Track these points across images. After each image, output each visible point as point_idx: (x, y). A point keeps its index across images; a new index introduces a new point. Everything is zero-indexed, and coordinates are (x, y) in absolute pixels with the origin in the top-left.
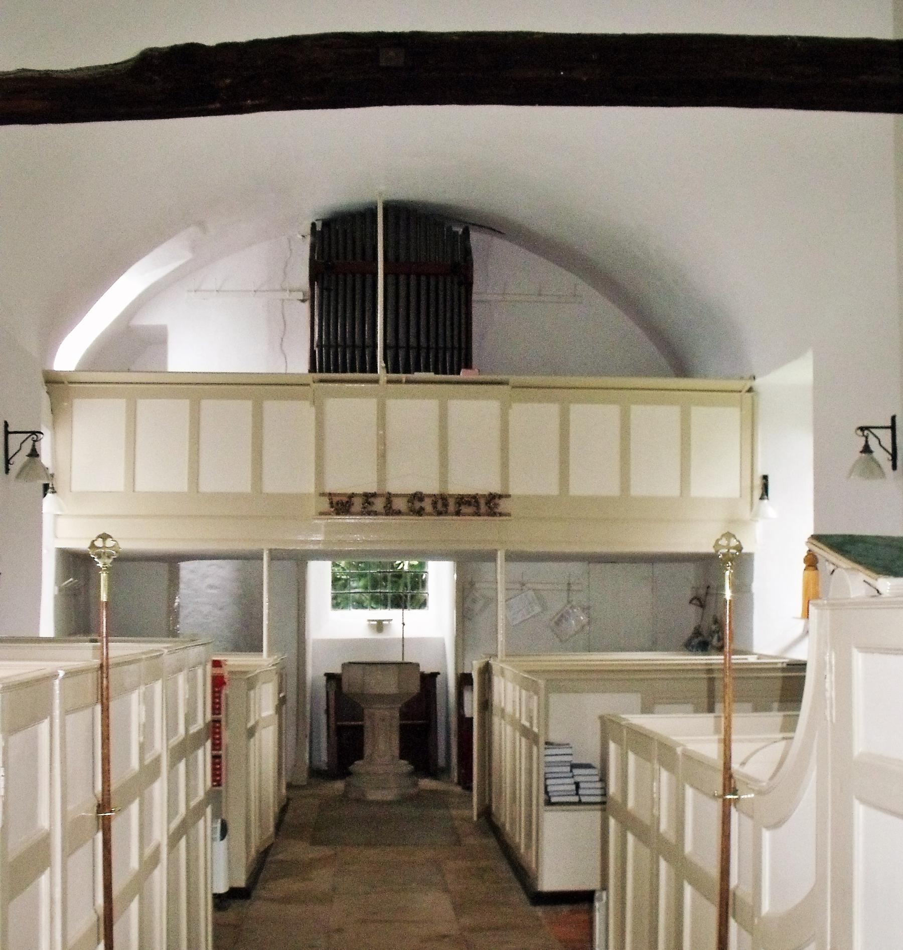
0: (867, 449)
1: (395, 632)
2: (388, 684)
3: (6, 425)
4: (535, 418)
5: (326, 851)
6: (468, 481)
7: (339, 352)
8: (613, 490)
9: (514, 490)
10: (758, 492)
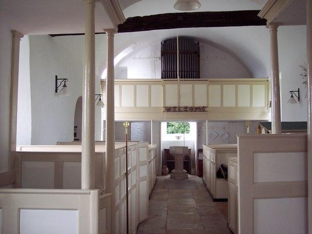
0: (292, 96)
1: (182, 139)
2: (181, 152)
3: (56, 76)
4: (215, 88)
5: (166, 190)
6: (199, 103)
7: (168, 74)
8: (234, 105)
9: (209, 106)
10: (269, 106)
